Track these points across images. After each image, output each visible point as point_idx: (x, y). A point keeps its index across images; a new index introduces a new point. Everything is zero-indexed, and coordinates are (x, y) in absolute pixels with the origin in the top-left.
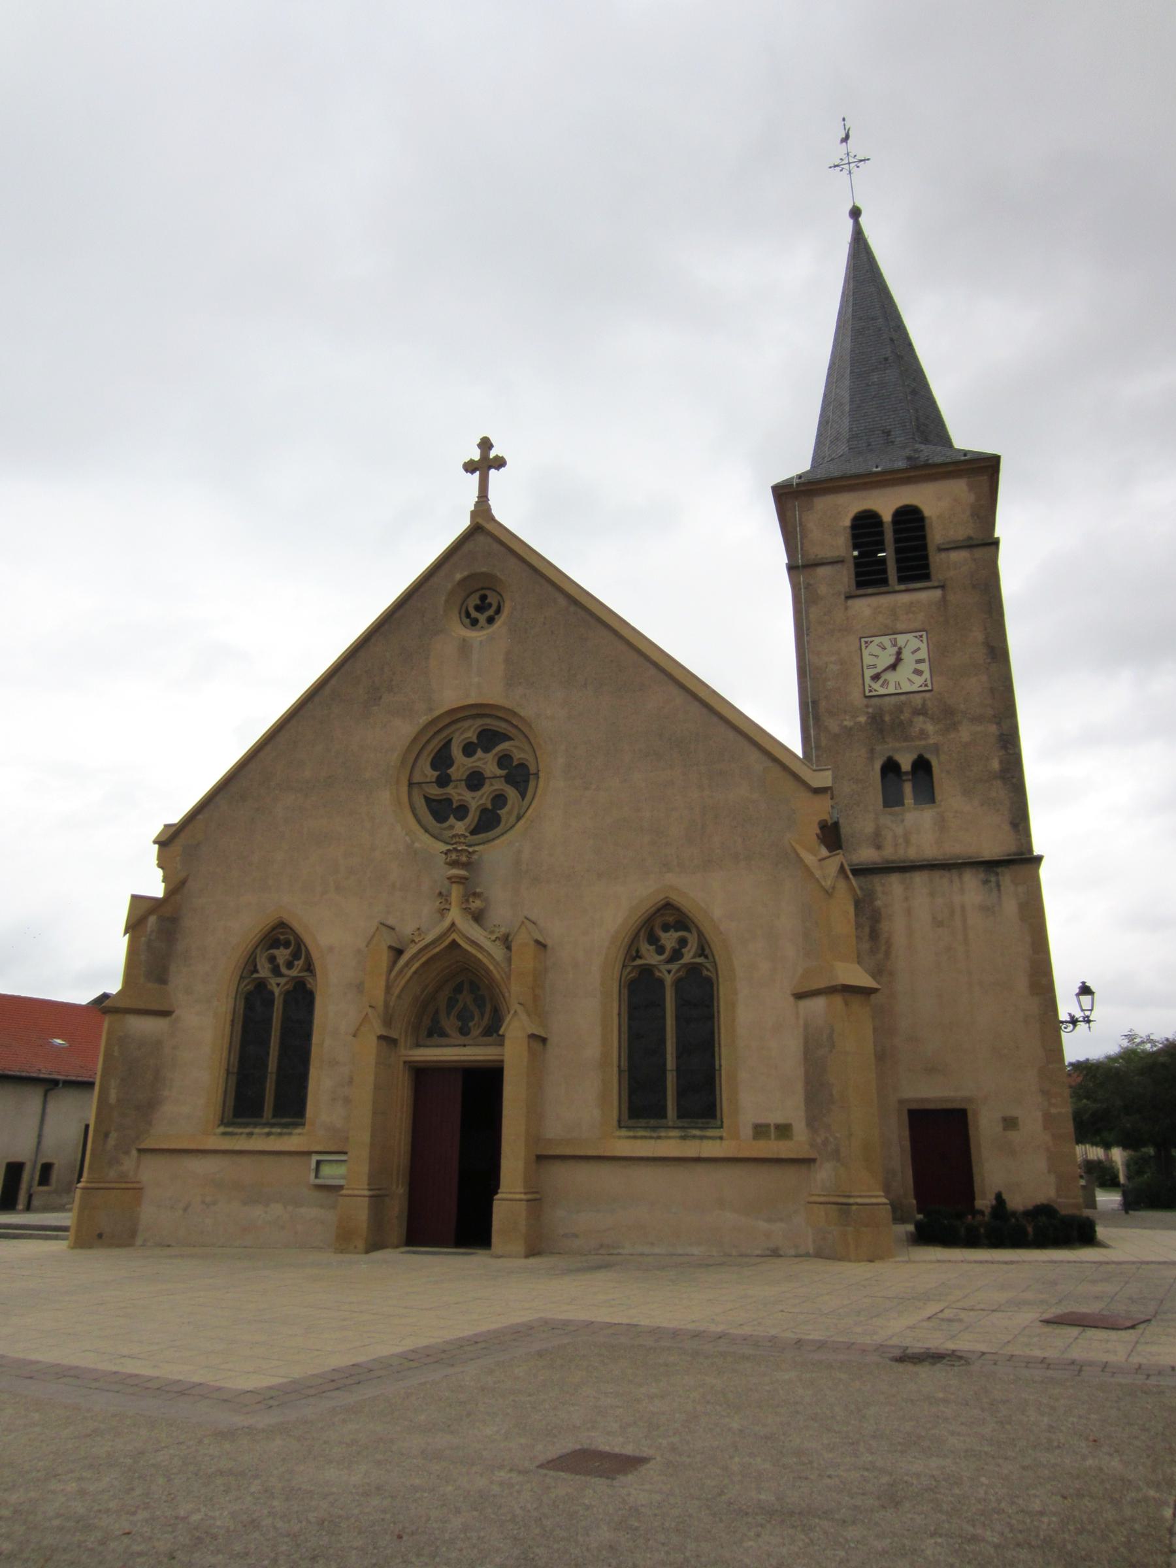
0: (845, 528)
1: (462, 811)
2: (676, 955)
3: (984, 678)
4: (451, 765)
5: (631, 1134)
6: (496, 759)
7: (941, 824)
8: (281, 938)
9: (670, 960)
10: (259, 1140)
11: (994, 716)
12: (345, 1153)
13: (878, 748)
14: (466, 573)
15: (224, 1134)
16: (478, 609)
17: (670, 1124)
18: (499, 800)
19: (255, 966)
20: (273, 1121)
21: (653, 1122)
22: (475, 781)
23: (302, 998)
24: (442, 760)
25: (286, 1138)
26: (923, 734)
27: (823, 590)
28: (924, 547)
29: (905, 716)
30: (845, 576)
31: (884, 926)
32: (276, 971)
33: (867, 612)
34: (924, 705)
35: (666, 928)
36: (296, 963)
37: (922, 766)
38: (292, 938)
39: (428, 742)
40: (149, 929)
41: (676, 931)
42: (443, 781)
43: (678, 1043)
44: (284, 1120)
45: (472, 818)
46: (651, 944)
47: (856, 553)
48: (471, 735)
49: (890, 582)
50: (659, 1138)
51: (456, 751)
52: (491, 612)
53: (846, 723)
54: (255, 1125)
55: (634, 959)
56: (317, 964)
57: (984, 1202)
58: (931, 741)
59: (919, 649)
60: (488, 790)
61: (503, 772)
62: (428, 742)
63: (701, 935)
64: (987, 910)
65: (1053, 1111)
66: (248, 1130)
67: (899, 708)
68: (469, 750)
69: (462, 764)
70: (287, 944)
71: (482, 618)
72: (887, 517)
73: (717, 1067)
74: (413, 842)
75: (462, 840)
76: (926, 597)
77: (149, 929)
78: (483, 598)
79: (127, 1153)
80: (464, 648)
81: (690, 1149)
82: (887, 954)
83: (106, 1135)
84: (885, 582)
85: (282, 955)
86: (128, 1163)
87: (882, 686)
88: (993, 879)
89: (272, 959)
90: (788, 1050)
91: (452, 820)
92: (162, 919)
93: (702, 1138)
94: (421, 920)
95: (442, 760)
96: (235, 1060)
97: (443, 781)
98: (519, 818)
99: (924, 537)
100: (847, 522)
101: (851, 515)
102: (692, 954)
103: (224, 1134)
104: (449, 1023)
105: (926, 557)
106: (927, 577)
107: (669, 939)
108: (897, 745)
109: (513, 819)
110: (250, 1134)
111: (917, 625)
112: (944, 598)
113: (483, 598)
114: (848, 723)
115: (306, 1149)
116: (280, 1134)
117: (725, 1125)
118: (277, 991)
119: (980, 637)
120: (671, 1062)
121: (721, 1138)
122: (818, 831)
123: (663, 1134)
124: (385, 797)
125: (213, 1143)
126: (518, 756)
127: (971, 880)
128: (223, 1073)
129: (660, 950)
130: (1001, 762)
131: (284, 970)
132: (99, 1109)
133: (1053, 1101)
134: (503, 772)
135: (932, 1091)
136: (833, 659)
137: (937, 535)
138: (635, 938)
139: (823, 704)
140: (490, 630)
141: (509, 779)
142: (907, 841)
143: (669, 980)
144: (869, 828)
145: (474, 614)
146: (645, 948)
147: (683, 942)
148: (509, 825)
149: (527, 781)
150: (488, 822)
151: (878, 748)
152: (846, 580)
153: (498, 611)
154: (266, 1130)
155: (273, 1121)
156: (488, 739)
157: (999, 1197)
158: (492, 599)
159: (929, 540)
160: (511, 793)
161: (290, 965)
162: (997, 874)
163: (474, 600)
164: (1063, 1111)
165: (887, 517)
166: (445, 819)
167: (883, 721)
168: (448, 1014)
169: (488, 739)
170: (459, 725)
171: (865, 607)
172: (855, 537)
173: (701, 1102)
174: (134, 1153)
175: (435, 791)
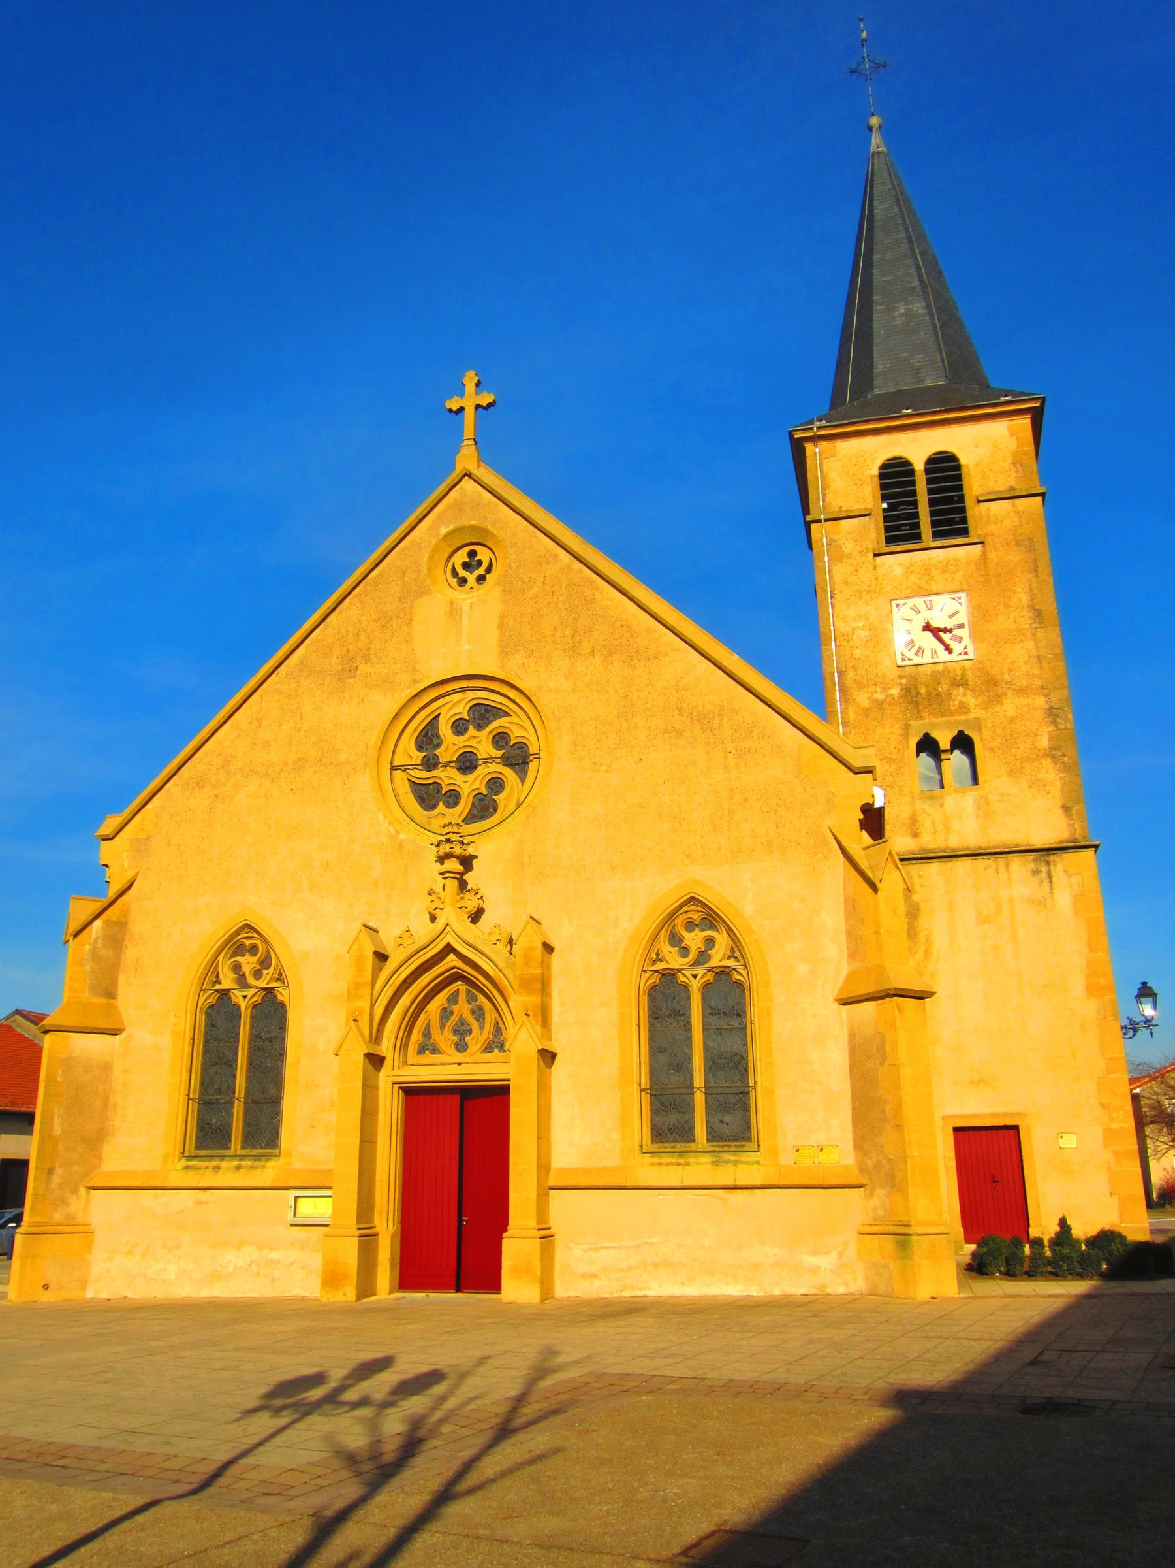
0: (872, 476)
1: (453, 798)
2: (702, 957)
3: (1030, 645)
4: (438, 746)
5: (656, 1160)
6: (491, 736)
7: (984, 811)
8: (244, 942)
9: (697, 963)
10: (227, 1172)
11: (1043, 688)
12: (330, 1188)
13: (913, 724)
14: (451, 527)
15: (187, 1168)
16: (466, 566)
17: (700, 1148)
18: (496, 784)
19: (217, 976)
20: (244, 1152)
21: (679, 1147)
22: (467, 763)
23: (272, 1013)
24: (428, 738)
25: (259, 1171)
26: (964, 708)
27: (848, 547)
28: (962, 499)
29: (943, 688)
30: (873, 530)
31: (923, 923)
32: (242, 982)
33: (898, 571)
34: (963, 674)
35: (690, 926)
36: (265, 972)
37: (963, 743)
38: (258, 942)
39: (410, 721)
40: (94, 936)
41: (702, 930)
42: (430, 763)
43: (706, 1058)
44: (256, 1152)
45: (464, 806)
46: (673, 945)
47: (885, 505)
48: (462, 710)
49: (923, 536)
50: (688, 1164)
51: (445, 729)
52: (481, 571)
53: (876, 696)
54: (222, 1157)
55: (654, 962)
56: (289, 974)
57: (1043, 1226)
58: (972, 716)
59: (957, 613)
60: (483, 772)
61: (500, 753)
62: (410, 721)
63: (730, 932)
64: (1039, 904)
65: (1115, 1126)
66: (215, 1163)
67: (936, 677)
68: (459, 727)
69: (451, 746)
70: (254, 950)
71: (472, 578)
72: (919, 466)
73: (751, 1083)
74: (398, 833)
75: (456, 829)
76: (960, 554)
77: (94, 936)
78: (472, 554)
79: (75, 1191)
80: (453, 612)
81: (726, 1175)
82: (927, 953)
83: (51, 1172)
84: (917, 537)
85: (248, 963)
86: (76, 1204)
87: (916, 654)
88: (1044, 869)
89: (237, 968)
90: (832, 1063)
91: (441, 807)
92: (108, 923)
93: (736, 1163)
94: (410, 921)
95: (428, 738)
96: (195, 1084)
97: (430, 763)
98: (519, 805)
99: (960, 488)
100: (875, 471)
101: (879, 463)
102: (719, 956)
103: (187, 1168)
104: (444, 1038)
105: (963, 510)
106: (965, 532)
107: (694, 940)
108: (935, 720)
109: (512, 807)
110: (217, 1168)
111: (956, 586)
112: (984, 553)
113: (472, 554)
114: (880, 696)
115: (283, 1185)
116: (252, 1167)
117: (762, 1148)
118: (243, 1004)
119: (1025, 599)
120: (699, 1080)
121: (758, 1163)
122: (861, 816)
123: (691, 1160)
124: (364, 781)
125: (175, 1179)
126: (516, 734)
127: (1019, 866)
128: (182, 1099)
129: (685, 951)
130: (1050, 739)
131: (251, 980)
132: (42, 1141)
133: (1115, 1115)
134: (500, 753)
135: (981, 1108)
136: (860, 624)
137: (974, 485)
138: (655, 937)
139: (850, 675)
140: (482, 591)
141: (508, 762)
142: (947, 828)
143: (695, 986)
144: (905, 814)
145: (462, 573)
146: (666, 949)
147: (710, 942)
148: (506, 814)
149: (526, 763)
150: (483, 808)
151: (913, 724)
152: (873, 535)
153: (489, 570)
154: (236, 1163)
155: (244, 1152)
156: (483, 714)
157: (1063, 1223)
158: (483, 554)
159: (966, 491)
160: (509, 775)
161: (257, 974)
162: (1048, 863)
163: (461, 557)
164: (1126, 1125)
165: (919, 466)
166: (434, 807)
167: (918, 693)
168: (443, 1026)
169: (483, 714)
170: (447, 699)
171: (897, 564)
172: (883, 487)
173: (734, 1121)
174: (82, 1191)
175: (421, 775)
